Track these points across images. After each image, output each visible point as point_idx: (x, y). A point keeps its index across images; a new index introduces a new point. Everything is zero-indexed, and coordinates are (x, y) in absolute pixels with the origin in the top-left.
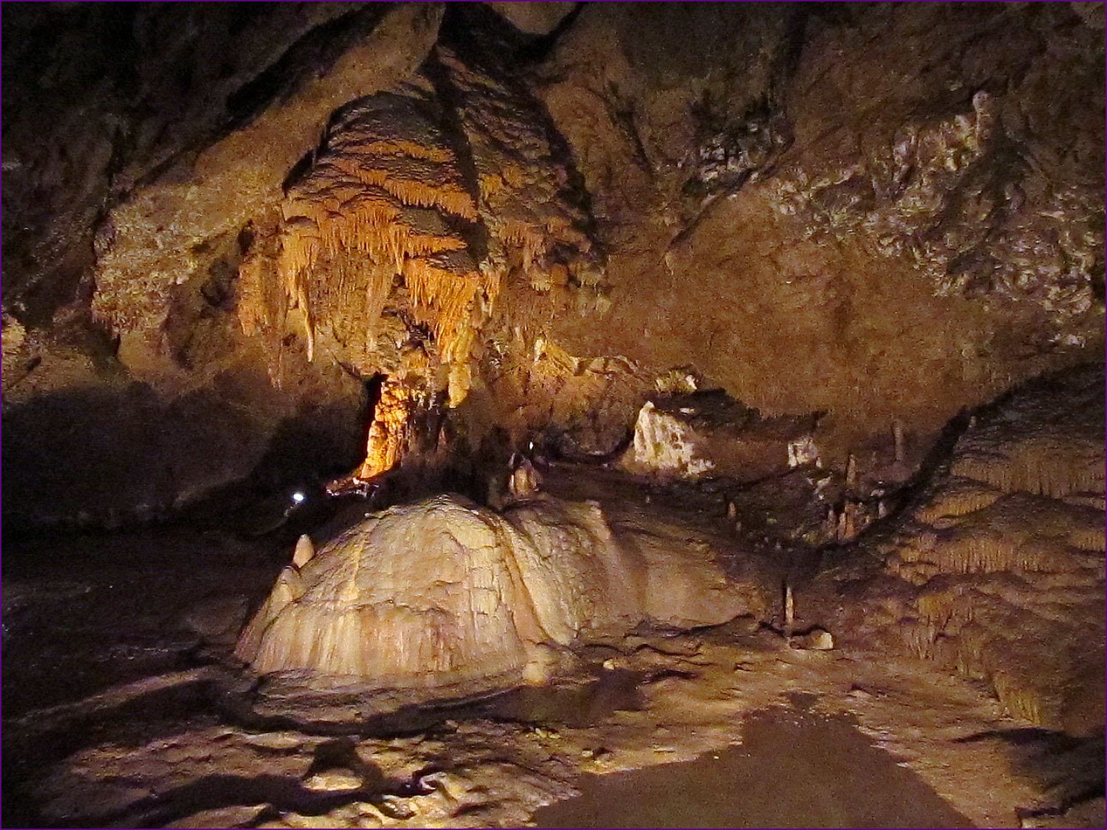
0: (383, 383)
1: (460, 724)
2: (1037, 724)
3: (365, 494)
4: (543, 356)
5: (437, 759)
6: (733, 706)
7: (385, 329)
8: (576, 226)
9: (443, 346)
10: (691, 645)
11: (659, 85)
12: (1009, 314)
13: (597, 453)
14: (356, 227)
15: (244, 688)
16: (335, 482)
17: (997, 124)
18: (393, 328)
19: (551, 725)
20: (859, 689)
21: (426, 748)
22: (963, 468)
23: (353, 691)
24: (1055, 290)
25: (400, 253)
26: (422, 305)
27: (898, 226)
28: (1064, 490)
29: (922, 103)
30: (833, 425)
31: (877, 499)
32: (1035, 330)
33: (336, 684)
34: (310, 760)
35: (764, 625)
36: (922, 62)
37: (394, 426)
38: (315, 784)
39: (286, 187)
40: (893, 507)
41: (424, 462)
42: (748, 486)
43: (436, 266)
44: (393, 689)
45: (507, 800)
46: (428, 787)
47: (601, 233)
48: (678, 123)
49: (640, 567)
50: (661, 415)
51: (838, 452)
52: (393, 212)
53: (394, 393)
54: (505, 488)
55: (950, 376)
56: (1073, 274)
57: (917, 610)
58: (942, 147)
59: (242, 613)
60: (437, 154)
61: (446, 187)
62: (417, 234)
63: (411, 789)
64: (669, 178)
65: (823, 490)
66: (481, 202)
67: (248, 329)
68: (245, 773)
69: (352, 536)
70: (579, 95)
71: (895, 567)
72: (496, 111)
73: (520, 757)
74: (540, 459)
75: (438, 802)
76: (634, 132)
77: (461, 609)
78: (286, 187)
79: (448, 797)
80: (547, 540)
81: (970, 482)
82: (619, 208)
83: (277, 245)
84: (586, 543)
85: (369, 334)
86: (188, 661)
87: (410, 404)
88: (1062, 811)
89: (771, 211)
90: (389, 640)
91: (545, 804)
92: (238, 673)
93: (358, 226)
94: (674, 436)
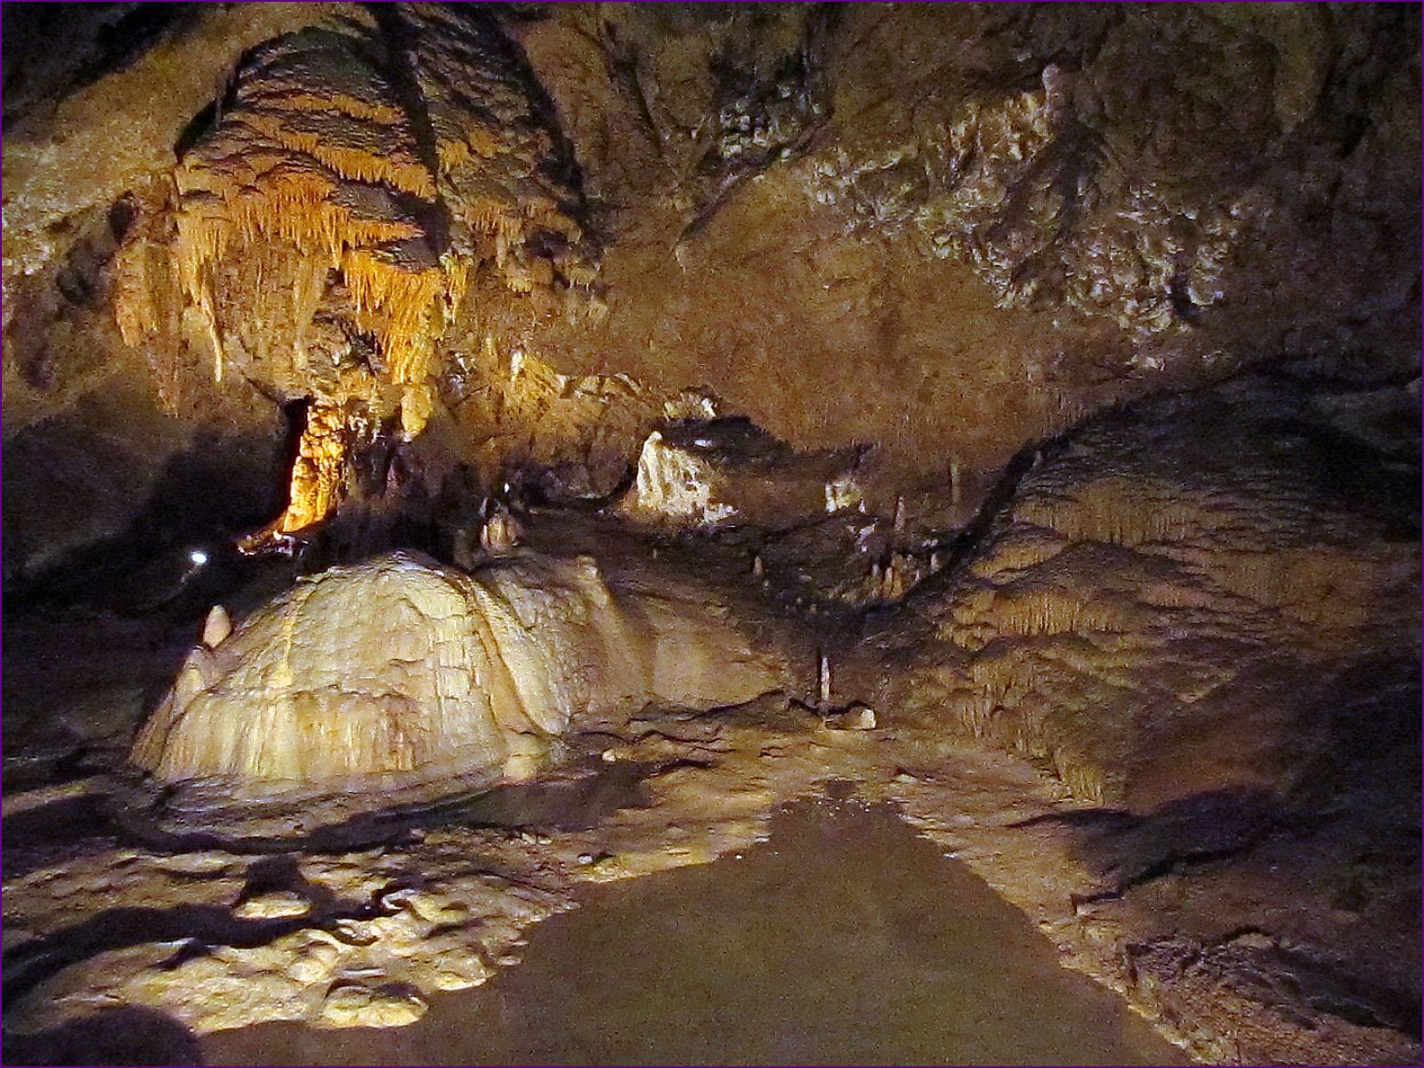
0: (310, 408)
1: (428, 832)
2: (1099, 803)
3: (290, 552)
4: (522, 373)
5: (404, 874)
6: (758, 799)
7: (318, 340)
8: (564, 209)
9: (396, 362)
10: (708, 729)
11: (666, 28)
12: (1082, 330)
13: (590, 496)
14: (278, 206)
15: (146, 801)
16: (249, 537)
17: (1069, 104)
18: (328, 339)
19: (541, 829)
20: (905, 773)
21: (388, 862)
22: (1026, 513)
23: (292, 800)
24: (1131, 305)
25: (337, 242)
26: (367, 310)
27: (955, 221)
28: (1137, 536)
29: (983, 75)
30: (878, 462)
31: (930, 551)
32: (1109, 351)
33: (269, 790)
34: (242, 884)
35: (794, 703)
36: (984, 24)
37: (326, 463)
38: (248, 913)
39: (181, 150)
40: (949, 556)
41: (369, 508)
42: (781, 535)
43: (383, 260)
44: (340, 795)
45: (487, 917)
46: (392, 907)
47: (594, 217)
48: (692, 80)
49: (647, 637)
50: (671, 448)
51: (886, 493)
52: (328, 189)
53: (325, 420)
54: (475, 543)
55: (1013, 400)
56: (1152, 285)
57: (971, 679)
58: (1006, 130)
59: (135, 708)
60: (386, 114)
61: (397, 157)
62: (361, 218)
63: (373, 911)
64: (681, 151)
65: (868, 539)
66: (440, 176)
67: (130, 339)
68: (158, 905)
69: (279, 606)
70: (565, 35)
71: (949, 631)
72: (459, 56)
73: (504, 867)
74: (518, 505)
75: (406, 924)
76: (638, 94)
77: (424, 694)
78: (181, 150)
79: (418, 918)
80: (529, 606)
81: (1035, 528)
82: (617, 188)
83: (168, 228)
84: (579, 609)
85: (296, 345)
86: (64, 772)
87: (346, 435)
88: (1118, 895)
89: (806, 198)
90: (335, 733)
91: (537, 919)
92: (136, 783)
93: (281, 206)
94: (687, 475)
